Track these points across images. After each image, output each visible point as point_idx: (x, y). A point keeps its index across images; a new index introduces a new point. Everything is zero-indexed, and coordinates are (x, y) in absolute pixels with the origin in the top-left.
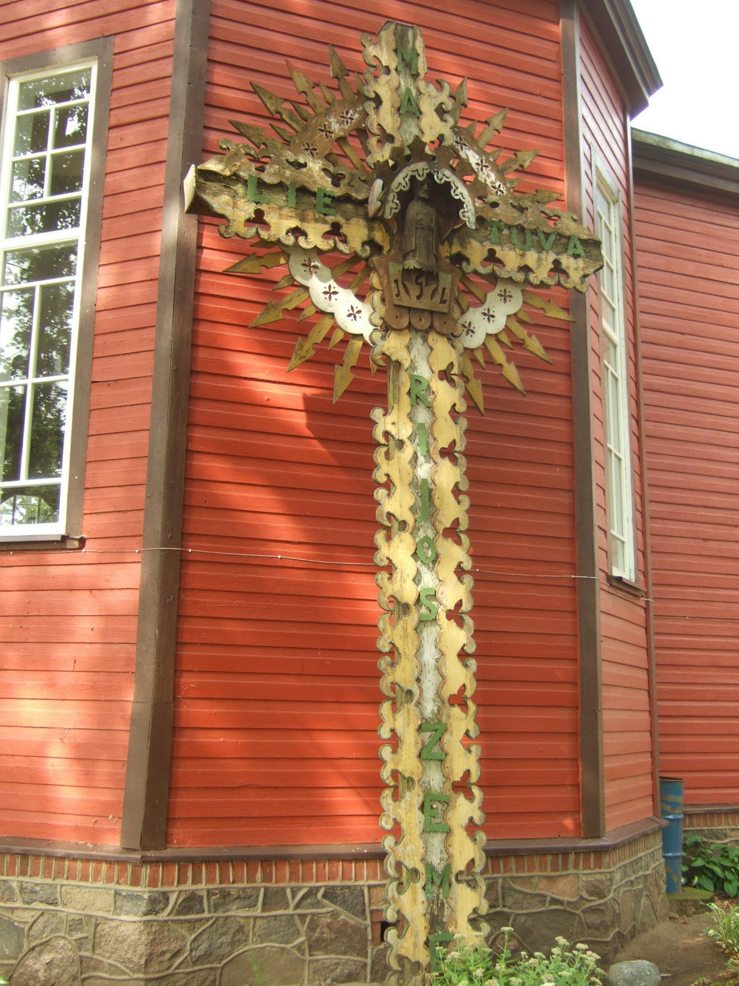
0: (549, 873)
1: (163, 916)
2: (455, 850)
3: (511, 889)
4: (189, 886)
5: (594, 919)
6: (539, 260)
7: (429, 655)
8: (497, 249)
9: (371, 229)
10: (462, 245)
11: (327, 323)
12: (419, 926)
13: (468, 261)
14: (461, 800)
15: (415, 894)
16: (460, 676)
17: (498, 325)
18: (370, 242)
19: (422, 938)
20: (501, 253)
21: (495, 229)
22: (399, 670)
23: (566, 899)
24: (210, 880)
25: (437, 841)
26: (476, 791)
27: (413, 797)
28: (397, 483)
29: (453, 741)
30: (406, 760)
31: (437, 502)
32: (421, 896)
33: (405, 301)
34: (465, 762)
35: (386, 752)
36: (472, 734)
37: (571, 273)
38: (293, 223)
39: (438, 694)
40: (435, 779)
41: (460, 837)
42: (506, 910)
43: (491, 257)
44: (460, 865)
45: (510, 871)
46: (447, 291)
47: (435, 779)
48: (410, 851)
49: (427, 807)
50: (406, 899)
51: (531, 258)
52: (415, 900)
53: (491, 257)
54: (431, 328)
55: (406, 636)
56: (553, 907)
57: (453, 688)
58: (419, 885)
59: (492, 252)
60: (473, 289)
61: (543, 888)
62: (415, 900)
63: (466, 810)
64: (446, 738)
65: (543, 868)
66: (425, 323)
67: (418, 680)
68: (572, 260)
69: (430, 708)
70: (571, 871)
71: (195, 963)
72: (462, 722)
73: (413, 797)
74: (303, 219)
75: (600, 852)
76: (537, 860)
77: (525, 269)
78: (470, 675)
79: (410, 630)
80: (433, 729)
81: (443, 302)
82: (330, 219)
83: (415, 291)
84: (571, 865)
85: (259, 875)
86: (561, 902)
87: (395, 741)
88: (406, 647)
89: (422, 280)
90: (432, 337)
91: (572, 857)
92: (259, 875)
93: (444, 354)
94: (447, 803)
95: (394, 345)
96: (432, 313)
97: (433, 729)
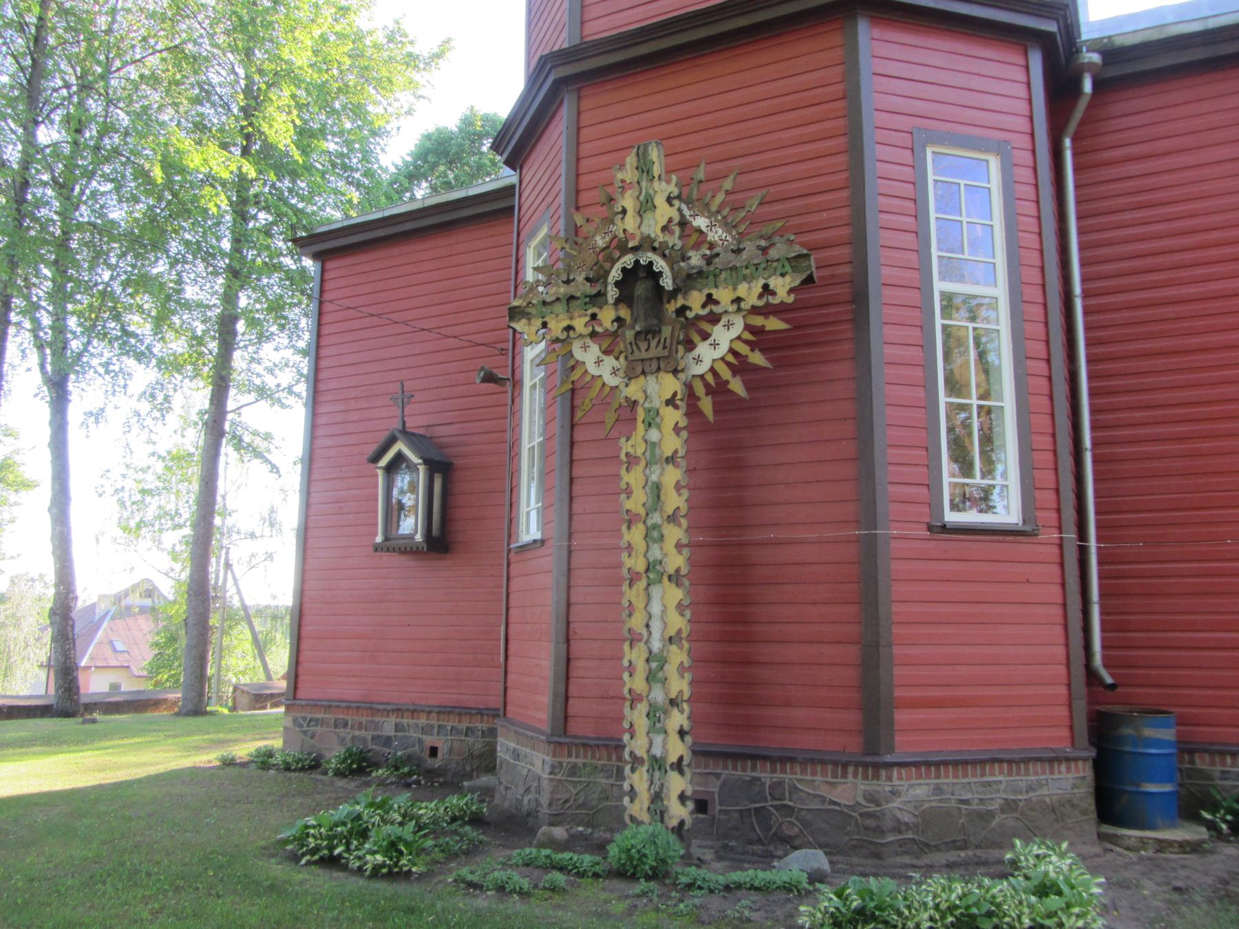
0: (830, 779)
1: (559, 777)
2: (670, 746)
3: (796, 788)
4: (573, 760)
5: (870, 822)
6: (750, 288)
7: (656, 608)
8: (714, 291)
9: (616, 310)
10: (684, 298)
11: (599, 384)
12: (644, 797)
13: (690, 309)
14: (675, 711)
15: (641, 775)
16: (678, 622)
17: (592, 370)
18: (618, 320)
19: (646, 805)
20: (716, 294)
21: (711, 277)
22: (633, 618)
23: (842, 802)
24: (586, 757)
25: (658, 739)
26: (685, 706)
27: (642, 708)
28: (634, 488)
29: (671, 669)
30: (638, 683)
31: (662, 497)
32: (646, 776)
33: (637, 355)
34: (680, 685)
35: (626, 676)
36: (686, 665)
37: (778, 291)
38: (566, 323)
39: (662, 636)
40: (658, 695)
41: (674, 738)
42: (791, 804)
43: (710, 300)
44: (673, 758)
45: (795, 773)
46: (668, 340)
47: (658, 695)
48: (638, 745)
49: (651, 715)
50: (636, 776)
51: (742, 290)
52: (641, 778)
53: (710, 300)
54: (659, 369)
55: (638, 595)
56: (833, 807)
57: (672, 632)
58: (645, 768)
59: (709, 296)
60: (694, 329)
61: (824, 791)
62: (641, 778)
63: (678, 719)
64: (666, 667)
65: (824, 774)
66: (654, 365)
67: (648, 626)
68: (780, 279)
69: (656, 645)
70: (850, 778)
71: (577, 808)
72: (678, 656)
73: (642, 708)
74: (571, 319)
75: (877, 767)
76: (749, 763)
77: (738, 300)
78: (685, 622)
79: (642, 592)
80: (657, 662)
81: (664, 348)
82: (590, 312)
83: (643, 346)
84: (850, 776)
85: (614, 757)
86: (839, 805)
87: (631, 669)
88: (639, 604)
89: (650, 336)
90: (662, 374)
91: (851, 769)
92: (614, 757)
93: (669, 385)
94: (666, 712)
95: (633, 391)
96: (658, 358)
97: (657, 662)
